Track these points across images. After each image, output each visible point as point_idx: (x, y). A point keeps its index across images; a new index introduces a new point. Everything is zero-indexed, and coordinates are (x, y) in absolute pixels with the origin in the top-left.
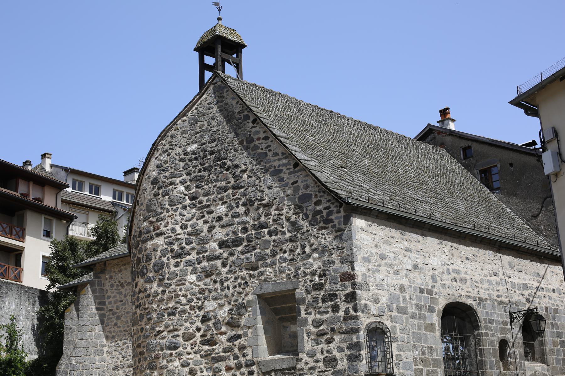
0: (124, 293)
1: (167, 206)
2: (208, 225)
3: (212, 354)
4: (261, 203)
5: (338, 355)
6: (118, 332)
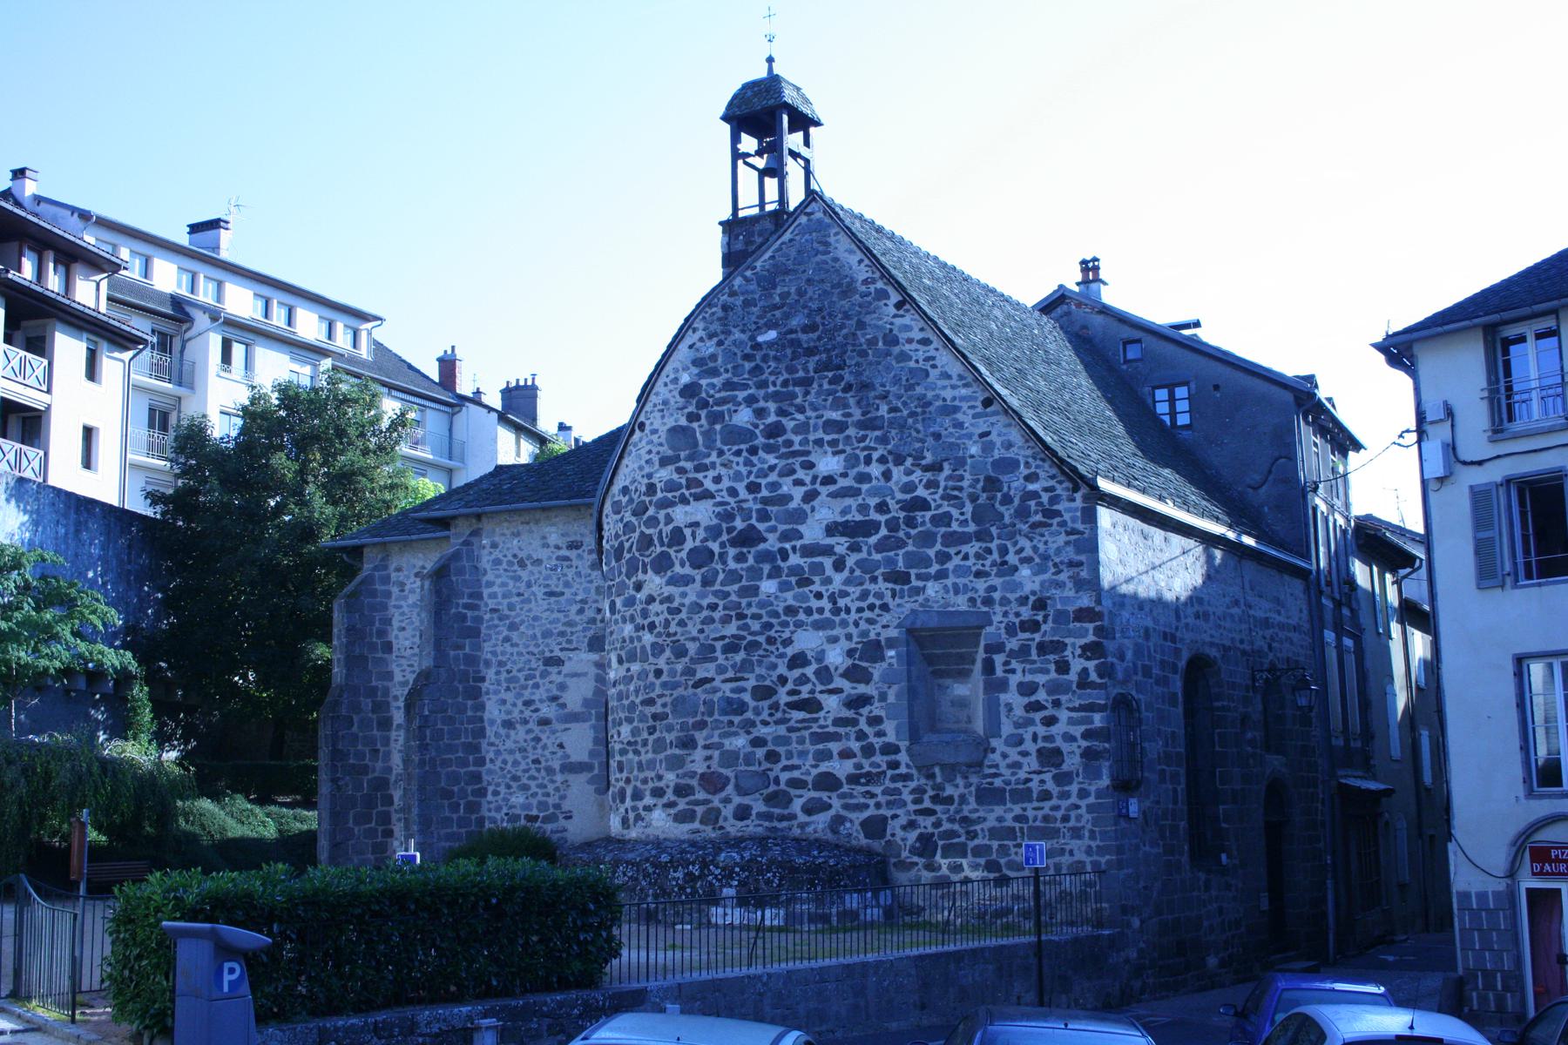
0: (525, 579)
1: (719, 444)
2: (804, 489)
5: (1065, 747)
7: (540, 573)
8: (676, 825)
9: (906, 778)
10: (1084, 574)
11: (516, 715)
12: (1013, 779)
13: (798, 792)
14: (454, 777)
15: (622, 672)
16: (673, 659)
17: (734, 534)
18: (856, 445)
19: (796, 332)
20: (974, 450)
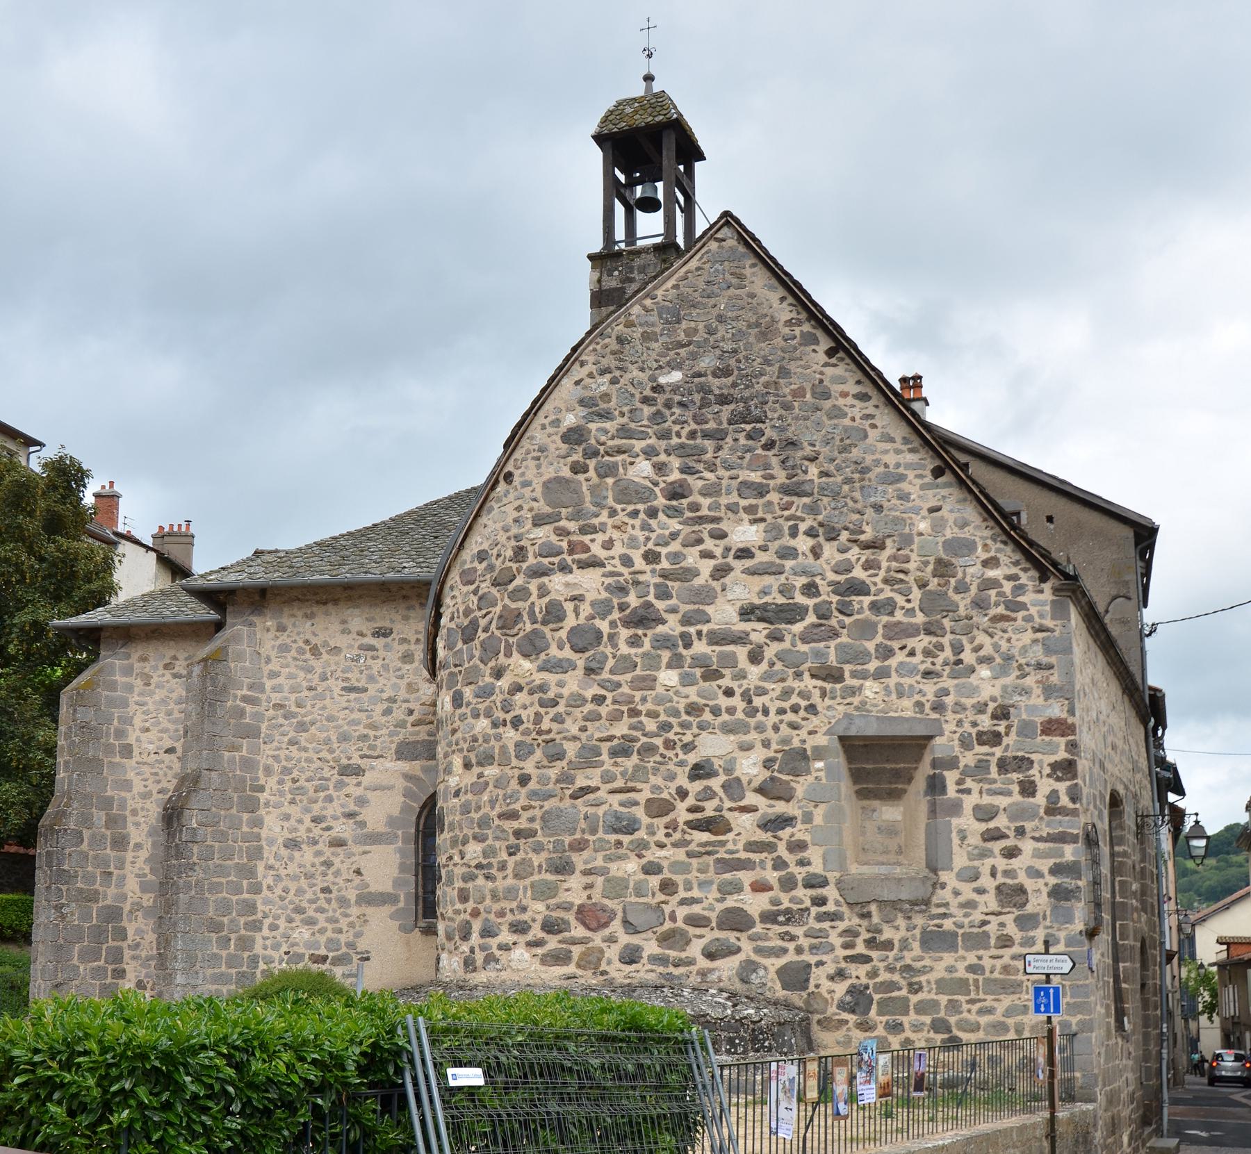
1: (610, 502)
2: (712, 562)
3: (717, 852)
4: (854, 537)
5: (1029, 884)
6: (299, 761)
7: (337, 664)
8: (544, 968)
9: (834, 917)
10: (1055, 679)
11: (302, 834)
12: (966, 921)
13: (698, 931)
14: (225, 907)
15: (470, 778)
16: (545, 763)
17: (628, 611)
18: (779, 513)
19: (705, 375)
20: (923, 526)
